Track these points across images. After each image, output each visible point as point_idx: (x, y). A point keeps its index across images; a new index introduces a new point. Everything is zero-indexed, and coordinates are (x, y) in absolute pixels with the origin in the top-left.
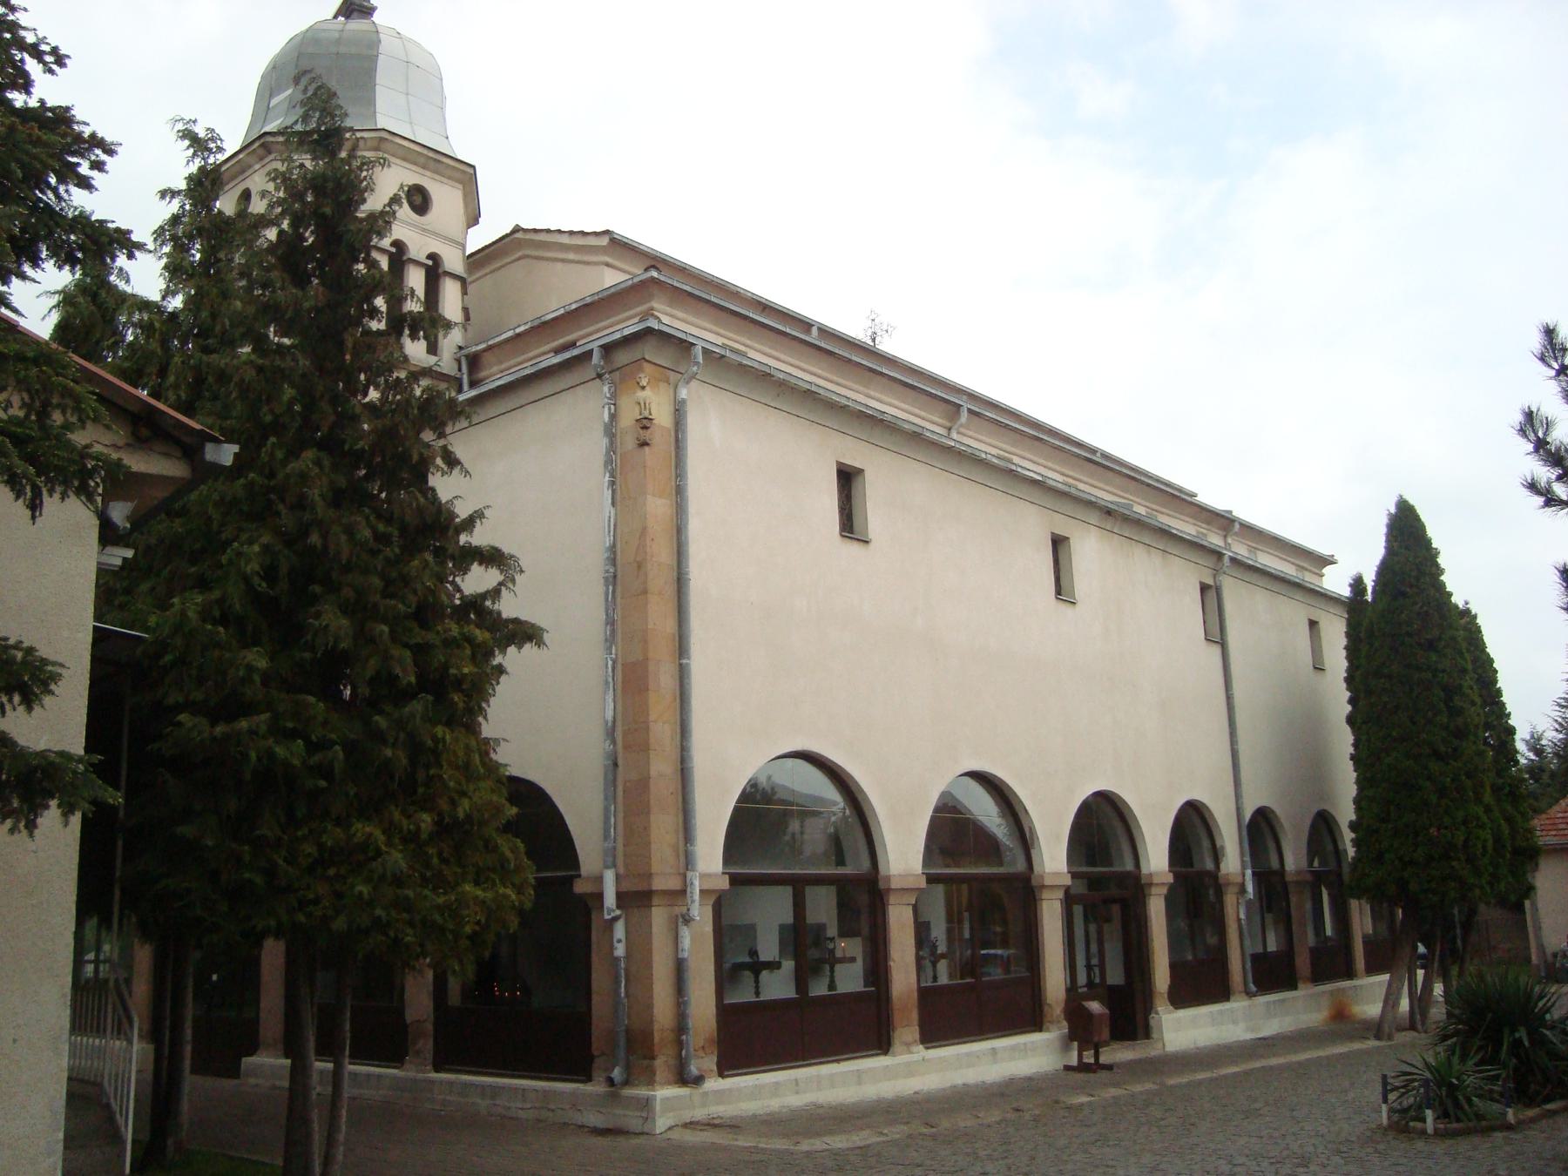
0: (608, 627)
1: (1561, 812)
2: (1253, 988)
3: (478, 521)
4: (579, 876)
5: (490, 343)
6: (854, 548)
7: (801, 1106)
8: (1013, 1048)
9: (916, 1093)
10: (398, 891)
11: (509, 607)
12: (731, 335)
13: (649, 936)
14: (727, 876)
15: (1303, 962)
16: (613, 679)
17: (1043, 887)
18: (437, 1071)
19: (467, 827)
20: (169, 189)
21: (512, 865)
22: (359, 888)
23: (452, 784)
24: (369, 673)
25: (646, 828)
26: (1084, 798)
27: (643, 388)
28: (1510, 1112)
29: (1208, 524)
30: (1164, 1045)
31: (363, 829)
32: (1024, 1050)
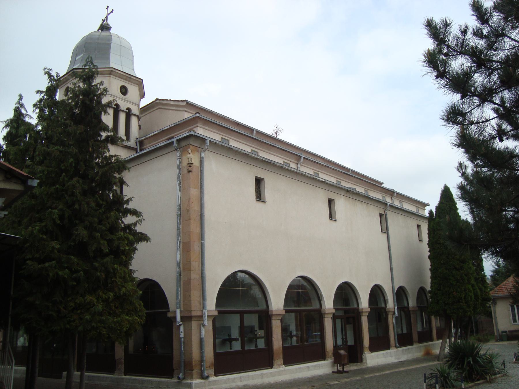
0: (178, 231)
1: (504, 285)
2: (398, 345)
3: (130, 201)
4: (169, 311)
5: (146, 137)
6: (260, 204)
7: (242, 386)
8: (315, 366)
9: (282, 381)
10: (101, 317)
11: (139, 229)
12: (223, 134)
13: (191, 330)
14: (217, 311)
15: (415, 336)
16: (180, 247)
17: (325, 313)
18: (125, 375)
19: (124, 297)
20: (40, 90)
21: (138, 310)
22: (87, 317)
23: (119, 283)
24: (94, 248)
25: (190, 296)
26: (339, 284)
27: (190, 153)
28: (463, 384)
29: (386, 193)
30: (367, 364)
31: (89, 298)
32: (319, 366)
